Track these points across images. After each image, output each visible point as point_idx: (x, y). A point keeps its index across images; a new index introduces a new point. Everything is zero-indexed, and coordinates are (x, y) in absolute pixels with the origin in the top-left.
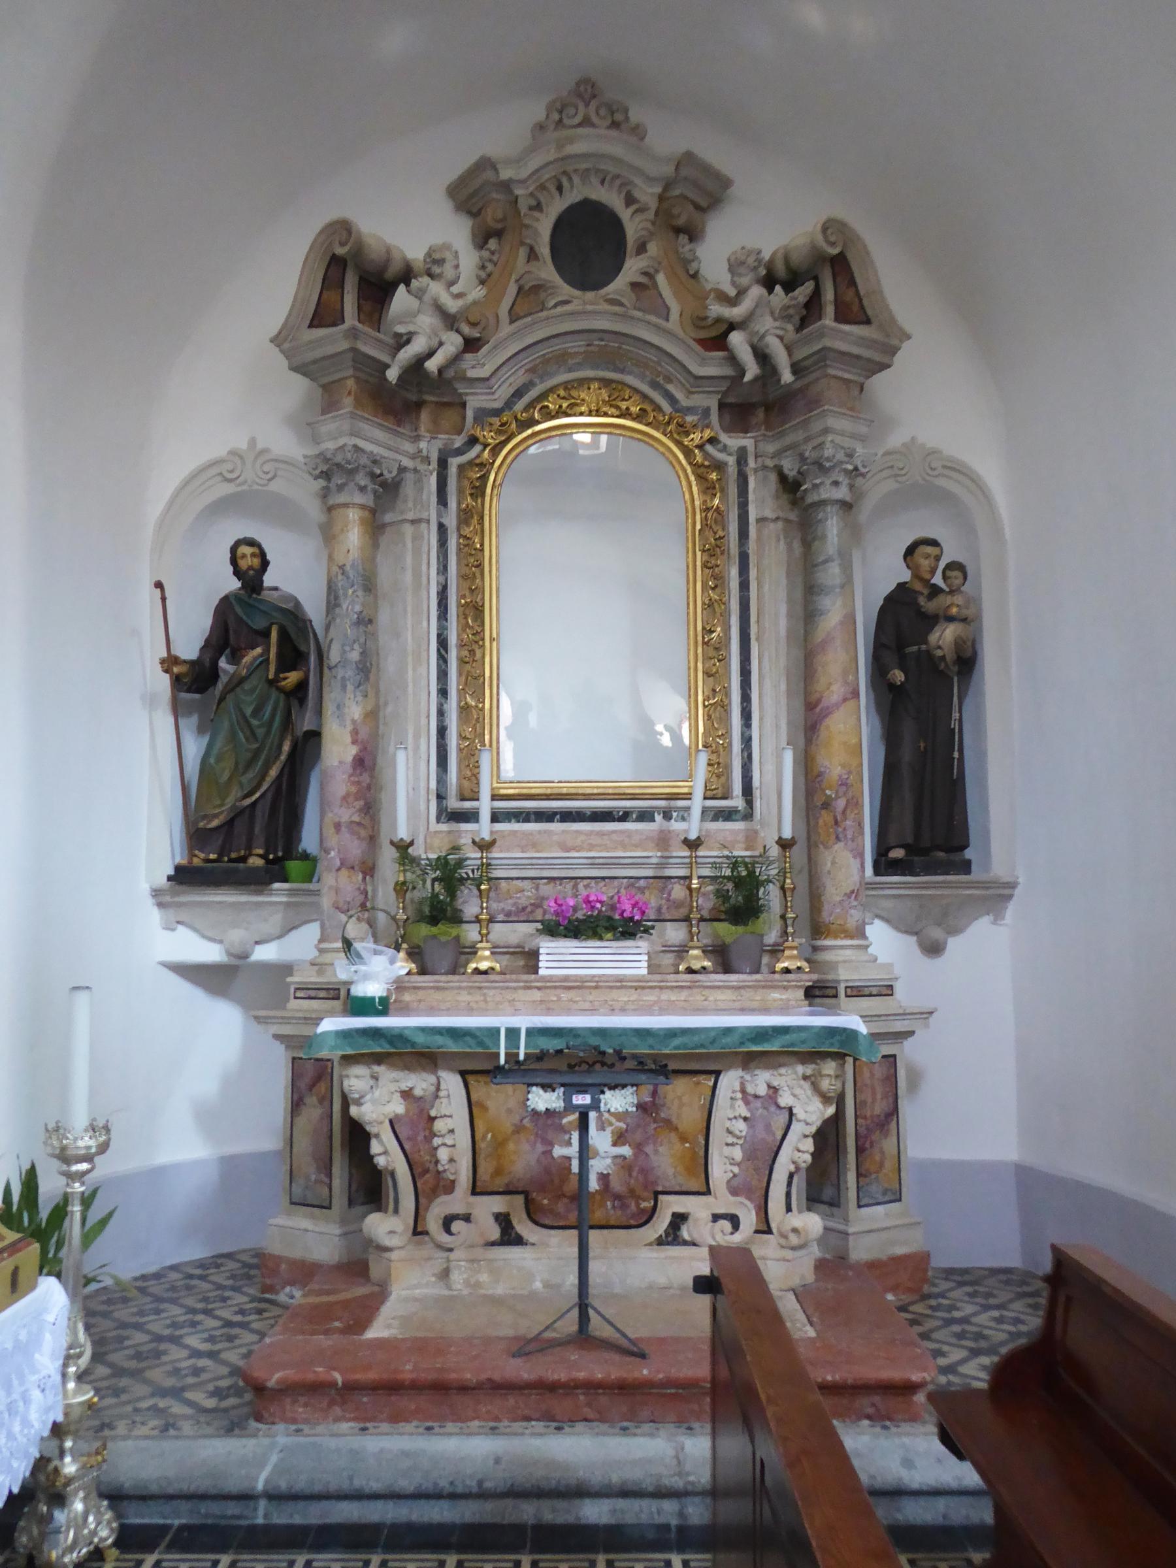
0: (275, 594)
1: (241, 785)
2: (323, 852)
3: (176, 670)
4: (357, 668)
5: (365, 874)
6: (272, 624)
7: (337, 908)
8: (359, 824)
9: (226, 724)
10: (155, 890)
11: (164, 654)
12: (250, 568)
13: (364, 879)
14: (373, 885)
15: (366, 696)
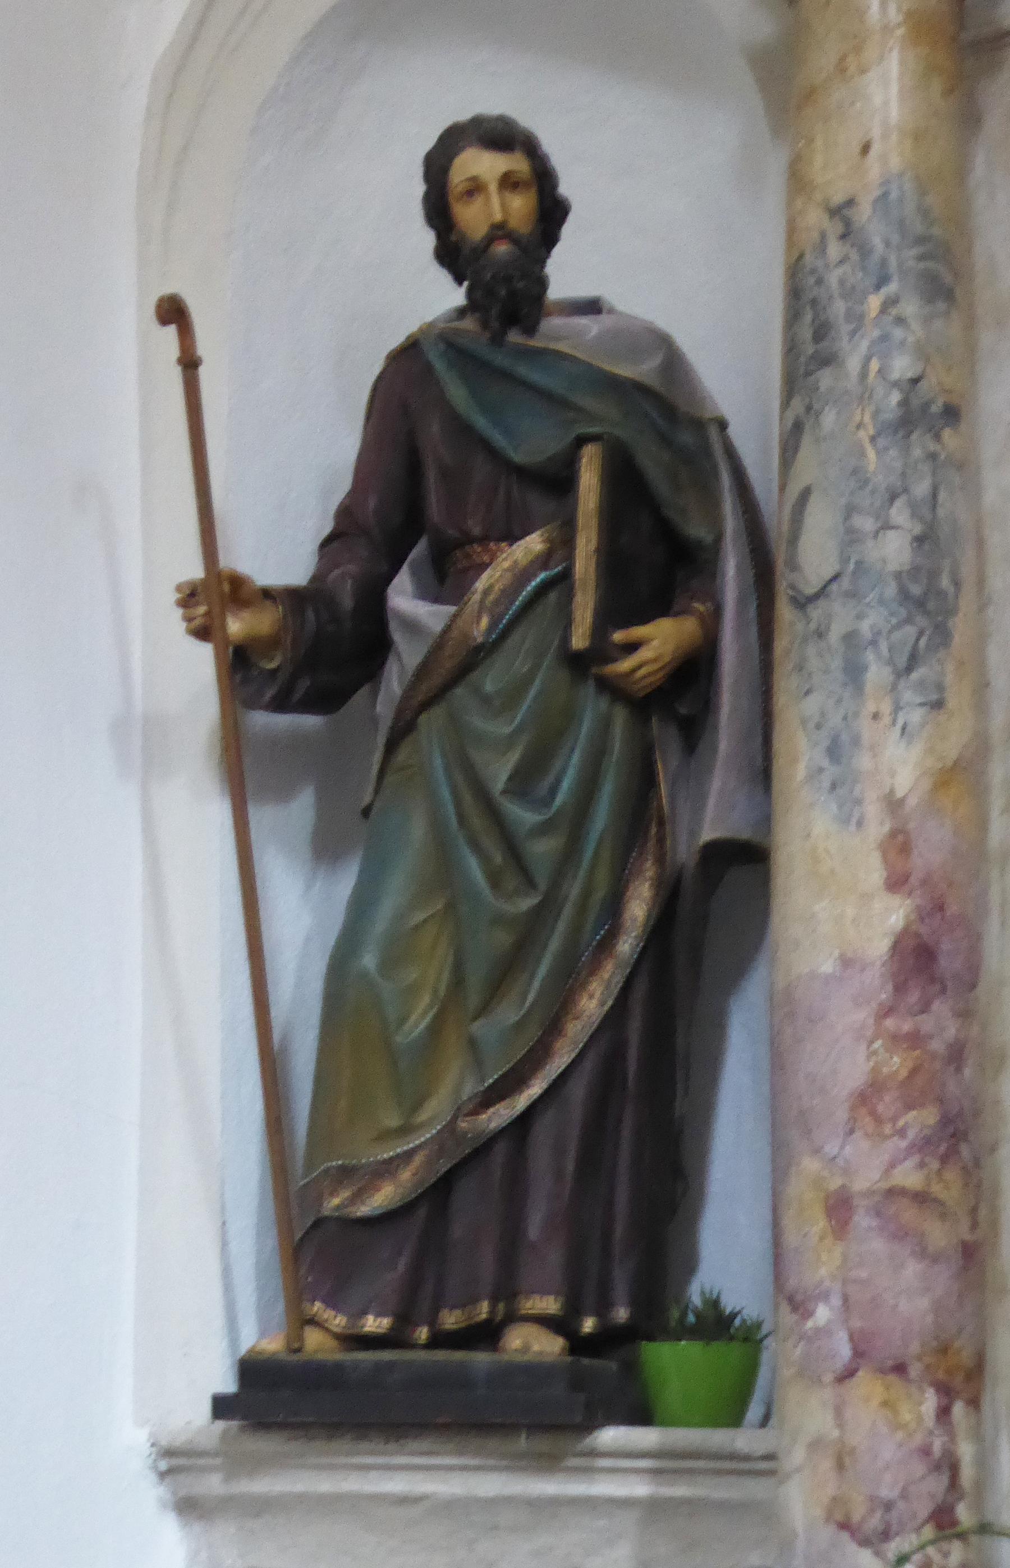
0: (591, 326)
1: (478, 1063)
2: (785, 1308)
3: (236, 626)
4: (904, 595)
5: (946, 1392)
6: (581, 441)
7: (844, 1526)
8: (921, 1198)
9: (418, 830)
10: (169, 1453)
11: (195, 571)
12: (499, 231)
13: (944, 1413)
14: (978, 1436)
15: (938, 705)
